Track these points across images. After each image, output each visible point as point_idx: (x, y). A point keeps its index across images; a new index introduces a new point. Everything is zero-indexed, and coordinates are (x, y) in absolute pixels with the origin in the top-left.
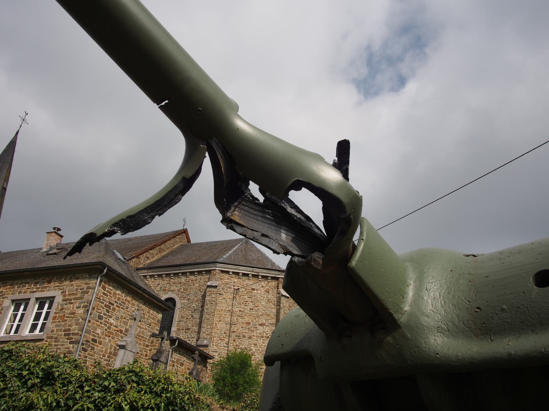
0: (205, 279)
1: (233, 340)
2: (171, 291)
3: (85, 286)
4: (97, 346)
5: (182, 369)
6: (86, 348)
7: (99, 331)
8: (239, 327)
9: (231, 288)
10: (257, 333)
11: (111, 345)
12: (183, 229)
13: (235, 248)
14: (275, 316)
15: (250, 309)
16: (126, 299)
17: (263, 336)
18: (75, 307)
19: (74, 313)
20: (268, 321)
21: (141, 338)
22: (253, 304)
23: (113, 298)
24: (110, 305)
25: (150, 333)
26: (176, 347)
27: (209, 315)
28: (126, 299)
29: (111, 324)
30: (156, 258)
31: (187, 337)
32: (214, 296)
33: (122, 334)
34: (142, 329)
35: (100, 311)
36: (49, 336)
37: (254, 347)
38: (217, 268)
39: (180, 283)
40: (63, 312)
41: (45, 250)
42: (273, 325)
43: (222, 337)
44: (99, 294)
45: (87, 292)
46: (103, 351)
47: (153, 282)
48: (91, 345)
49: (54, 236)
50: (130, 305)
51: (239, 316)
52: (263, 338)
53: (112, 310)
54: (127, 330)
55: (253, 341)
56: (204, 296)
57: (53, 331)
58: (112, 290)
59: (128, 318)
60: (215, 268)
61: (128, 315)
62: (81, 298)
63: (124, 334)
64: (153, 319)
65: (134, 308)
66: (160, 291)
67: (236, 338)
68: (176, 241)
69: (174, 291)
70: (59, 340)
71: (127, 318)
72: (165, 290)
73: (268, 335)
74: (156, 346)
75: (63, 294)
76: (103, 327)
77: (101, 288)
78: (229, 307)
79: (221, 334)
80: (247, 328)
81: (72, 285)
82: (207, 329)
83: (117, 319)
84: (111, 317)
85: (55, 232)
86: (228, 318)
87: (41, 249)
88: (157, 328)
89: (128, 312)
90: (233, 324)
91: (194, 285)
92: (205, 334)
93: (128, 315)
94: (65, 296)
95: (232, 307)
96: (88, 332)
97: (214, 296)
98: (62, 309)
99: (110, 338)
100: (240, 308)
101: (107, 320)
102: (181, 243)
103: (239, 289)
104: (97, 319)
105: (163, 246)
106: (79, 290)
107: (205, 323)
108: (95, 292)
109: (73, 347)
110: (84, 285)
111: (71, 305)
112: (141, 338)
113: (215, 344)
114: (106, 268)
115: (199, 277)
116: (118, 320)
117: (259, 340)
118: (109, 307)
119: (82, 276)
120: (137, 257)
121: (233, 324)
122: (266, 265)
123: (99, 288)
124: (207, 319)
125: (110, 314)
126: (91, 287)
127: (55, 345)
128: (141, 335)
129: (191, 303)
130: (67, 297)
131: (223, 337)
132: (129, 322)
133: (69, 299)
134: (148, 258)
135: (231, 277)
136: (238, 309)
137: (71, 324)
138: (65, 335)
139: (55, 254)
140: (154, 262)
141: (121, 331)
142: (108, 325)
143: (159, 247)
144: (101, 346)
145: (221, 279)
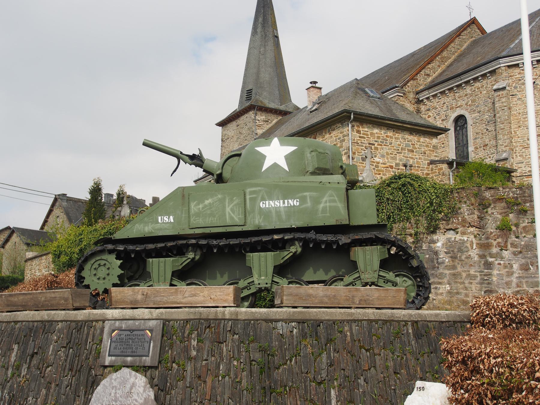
0: (492, 82)
3: (341, 135)
12: (471, 19)
16: (386, 136)
23: (371, 139)
25: (427, 162)
27: (503, 123)
28: (386, 136)
29: (378, 163)
30: (440, 71)
33: (394, 169)
34: (416, 160)
38: (502, 65)
39: (466, 95)
41: (310, 107)
43: (526, 144)
44: (356, 138)
45: (344, 140)
47: (438, 102)
49: (313, 91)
50: (394, 140)
53: (375, 149)
58: (367, 132)
59: (396, 153)
60: (499, 66)
63: (395, 168)
64: (427, 146)
65: (399, 142)
66: (448, 110)
68: (464, 39)
69: (462, 106)
71: (394, 153)
72: (452, 108)
74: (436, 172)
77: (355, 133)
82: (504, 140)
83: (383, 156)
85: (312, 87)
87: (307, 107)
91: (481, 93)
97: (504, 100)
99: (381, 175)
101: (373, 160)
105: (445, 54)
106: (338, 140)
107: (500, 134)
108: (350, 138)
113: (519, 154)
114: (352, 113)
115: (485, 82)
120: (413, 79)
123: (354, 133)
124: (502, 129)
128: (417, 165)
129: (483, 114)
132: (398, 156)
134: (428, 75)
139: (316, 109)
140: (437, 77)
142: (374, 164)
143: (439, 56)
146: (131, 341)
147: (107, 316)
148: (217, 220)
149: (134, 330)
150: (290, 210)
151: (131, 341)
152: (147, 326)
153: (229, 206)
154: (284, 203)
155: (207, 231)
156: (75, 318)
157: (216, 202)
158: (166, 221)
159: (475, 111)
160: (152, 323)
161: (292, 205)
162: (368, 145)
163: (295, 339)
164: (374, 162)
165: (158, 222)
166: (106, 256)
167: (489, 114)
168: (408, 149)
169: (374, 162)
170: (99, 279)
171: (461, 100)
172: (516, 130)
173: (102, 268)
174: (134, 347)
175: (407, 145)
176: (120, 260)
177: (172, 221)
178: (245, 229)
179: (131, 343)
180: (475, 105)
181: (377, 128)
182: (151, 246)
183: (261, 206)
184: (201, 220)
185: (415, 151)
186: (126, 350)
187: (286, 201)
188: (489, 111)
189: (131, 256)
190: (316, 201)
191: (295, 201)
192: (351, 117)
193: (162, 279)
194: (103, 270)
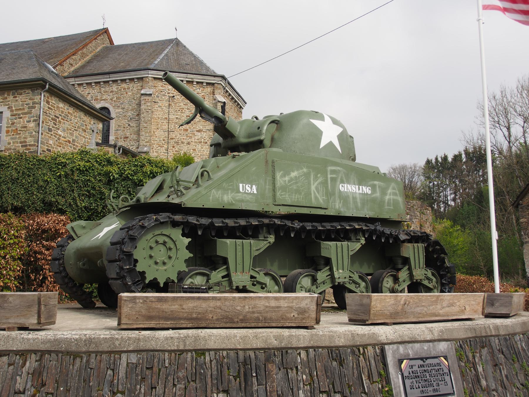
2: (103, 100)
3: (31, 102)
7: (51, 142)
8: (177, 134)
9: (166, 96)
10: (195, 139)
12: (104, 29)
13: (165, 52)
18: (26, 121)
19: (25, 127)
20: (205, 127)
22: (189, 111)
29: (60, 136)
30: (80, 64)
32: (149, 104)
33: (71, 144)
35: (49, 124)
38: (149, 76)
39: (112, 92)
50: (73, 117)
54: (74, 140)
55: (191, 147)
56: (139, 105)
57: (9, 144)
58: (55, 104)
60: (147, 76)
61: (73, 126)
62: (30, 113)
63: (72, 144)
67: (175, 145)
68: (98, 43)
69: (107, 100)
71: (72, 130)
81: (17, 100)
84: (59, 129)
86: (165, 125)
89: (72, 124)
91: (127, 93)
93: (73, 126)
94: (12, 111)
96: (42, 143)
97: (149, 104)
98: (13, 124)
100: (177, 115)
102: (103, 45)
103: (174, 96)
105: (85, 50)
106: (25, 106)
111: (21, 120)
114: (48, 84)
115: (132, 85)
118: (56, 121)
119: (25, 92)
122: (200, 71)
130: (14, 112)
131: (162, 144)
132: (74, 133)
133: (17, 114)
134: (71, 65)
135: (165, 84)
141: (69, 142)
142: (57, 136)
145: (155, 86)
146: (428, 375)
147: (380, 338)
148: (303, 198)
149: (427, 358)
152: (437, 350)
153: (314, 184)
154: (359, 189)
155: (292, 210)
156: (331, 342)
157: (302, 176)
158: (248, 191)
159: (119, 107)
160: (443, 346)
161: (366, 193)
162: (54, 117)
164: (57, 134)
165: (239, 192)
166: (169, 231)
167: (133, 113)
168: (82, 128)
169: (57, 134)
171: (107, 94)
173: (162, 248)
174: (435, 384)
175: (82, 125)
176: (187, 238)
177: (255, 192)
179: (428, 377)
180: (120, 102)
181: (62, 103)
182: (230, 222)
183: (341, 190)
184: (287, 196)
185: (87, 131)
186: (426, 389)
187: (361, 187)
188: (132, 110)
189: (198, 233)
190: (384, 192)
191: (368, 188)
192: (45, 87)
193: (240, 267)
194: (162, 250)
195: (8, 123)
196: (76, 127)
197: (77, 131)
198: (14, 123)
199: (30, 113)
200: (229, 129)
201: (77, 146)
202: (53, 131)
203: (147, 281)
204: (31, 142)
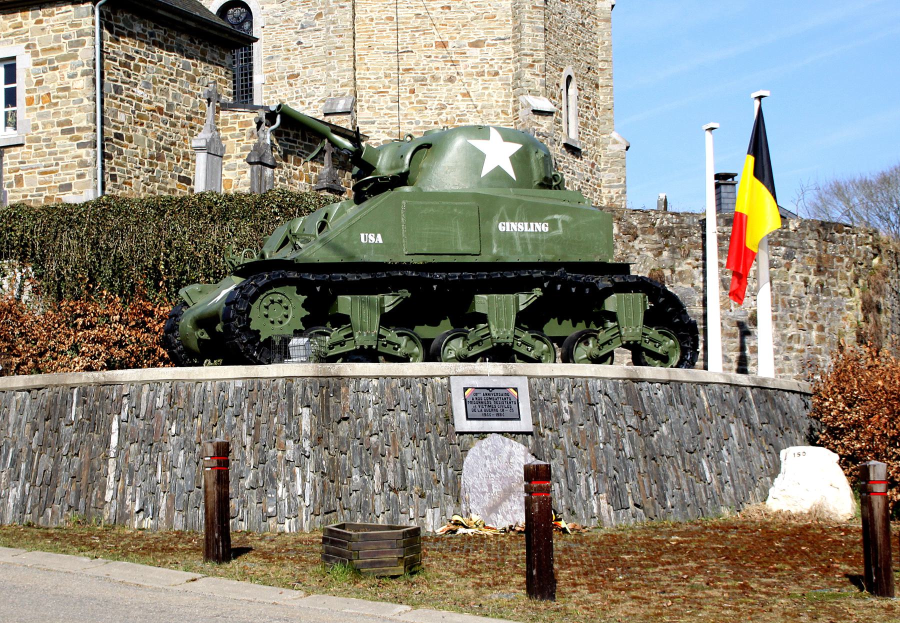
1: (408, 90)
4: (126, 146)
5: (300, 171)
6: (109, 152)
7: (121, 117)
10: (467, 66)
11: (149, 140)
14: (510, 18)
15: (443, 8)
16: (153, 41)
17: (484, 72)
18: (66, 76)
21: (199, 116)
24: (129, 61)
26: (279, 127)
27: (341, 36)
29: (140, 100)
31: (295, 95)
34: (198, 99)
36: (30, 138)
37: (462, 100)
40: (42, 88)
42: (507, 41)
43: (381, 86)
46: (138, 153)
48: (116, 146)
51: (417, 29)
52: (484, 76)
57: (35, 128)
59: (167, 81)
61: (166, 73)
63: (166, 114)
67: (416, 86)
70: (55, 144)
73: (496, 69)
74: (235, 129)
75: (30, 50)
76: (126, 108)
78: (388, 11)
79: (377, 78)
80: (441, 56)
81: (43, 29)
83: (147, 85)
86: (388, 37)
88: (228, 89)
90: (404, 52)
92: (339, 84)
93: (166, 73)
94: (35, 54)
95: (395, 10)
98: (39, 83)
99: (145, 127)
104: (113, 93)
106: (63, 40)
109: (88, 154)
110: (70, 29)
111: (57, 72)
112: (199, 116)
116: (149, 89)
117: (474, 82)
121: (404, 52)
124: (337, 48)
125: (132, 80)
126: (85, 31)
127: (50, 154)
128: (199, 111)
129: (291, 8)
130: (41, 57)
132: (170, 87)
136: (410, 11)
137: (68, 110)
138: (63, 132)
141: (160, 110)
144: (133, 145)
146: (493, 402)
149: (493, 389)
150: (536, 240)
151: (493, 402)
154: (529, 226)
155: (430, 259)
161: (540, 231)
162: (123, 58)
163: (662, 402)
167: (306, 10)
168: (187, 74)
170: (281, 323)
172: (363, 52)
174: (499, 409)
176: (303, 295)
177: (381, 241)
178: (478, 259)
179: (493, 403)
183: (500, 229)
187: (532, 224)
191: (544, 224)
195: (28, 83)
196: (172, 74)
197: (175, 81)
198: (43, 80)
199: (75, 57)
200: (367, 161)
201: (178, 118)
202: (125, 92)
203: (262, 340)
204: (81, 121)
